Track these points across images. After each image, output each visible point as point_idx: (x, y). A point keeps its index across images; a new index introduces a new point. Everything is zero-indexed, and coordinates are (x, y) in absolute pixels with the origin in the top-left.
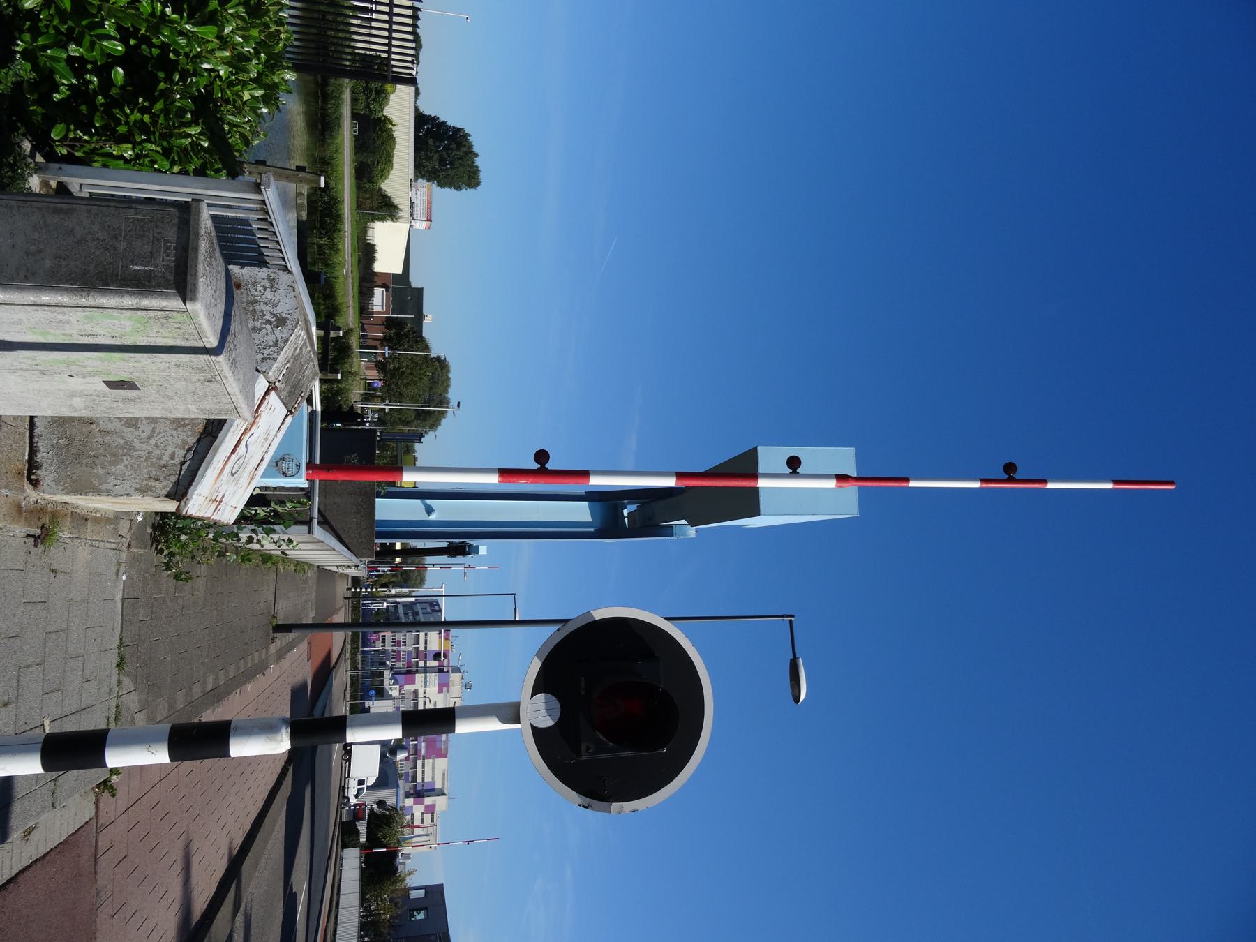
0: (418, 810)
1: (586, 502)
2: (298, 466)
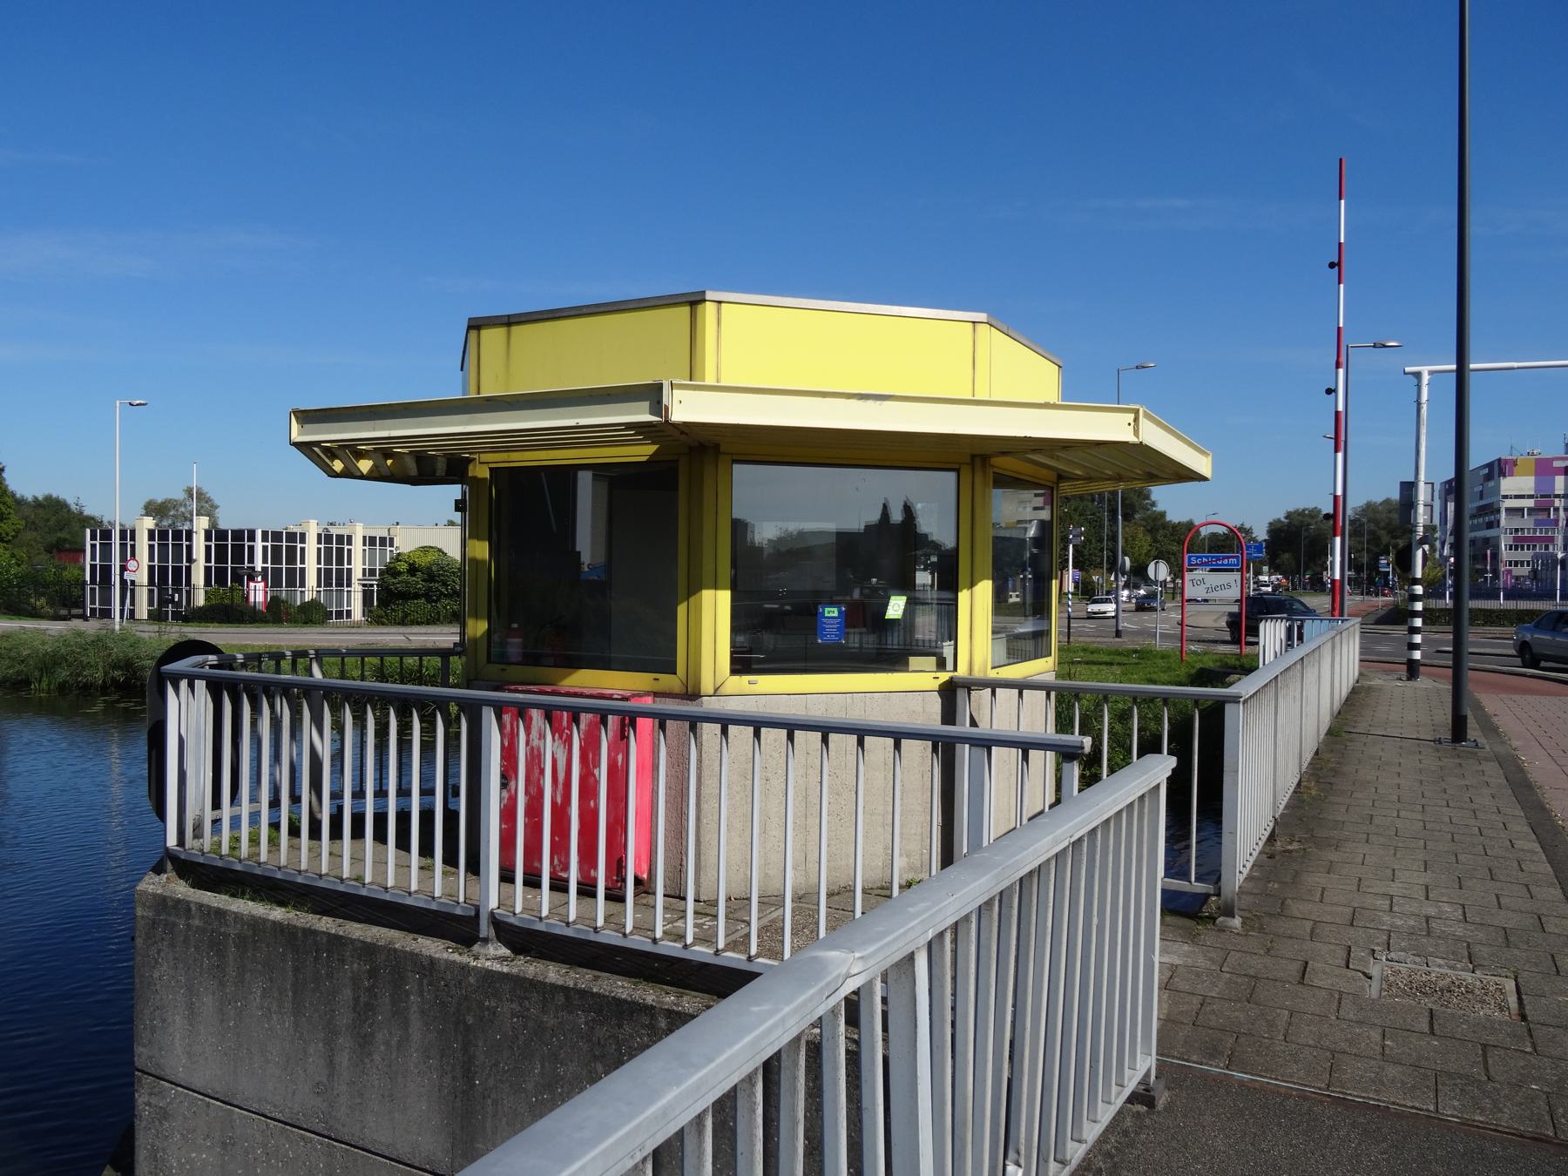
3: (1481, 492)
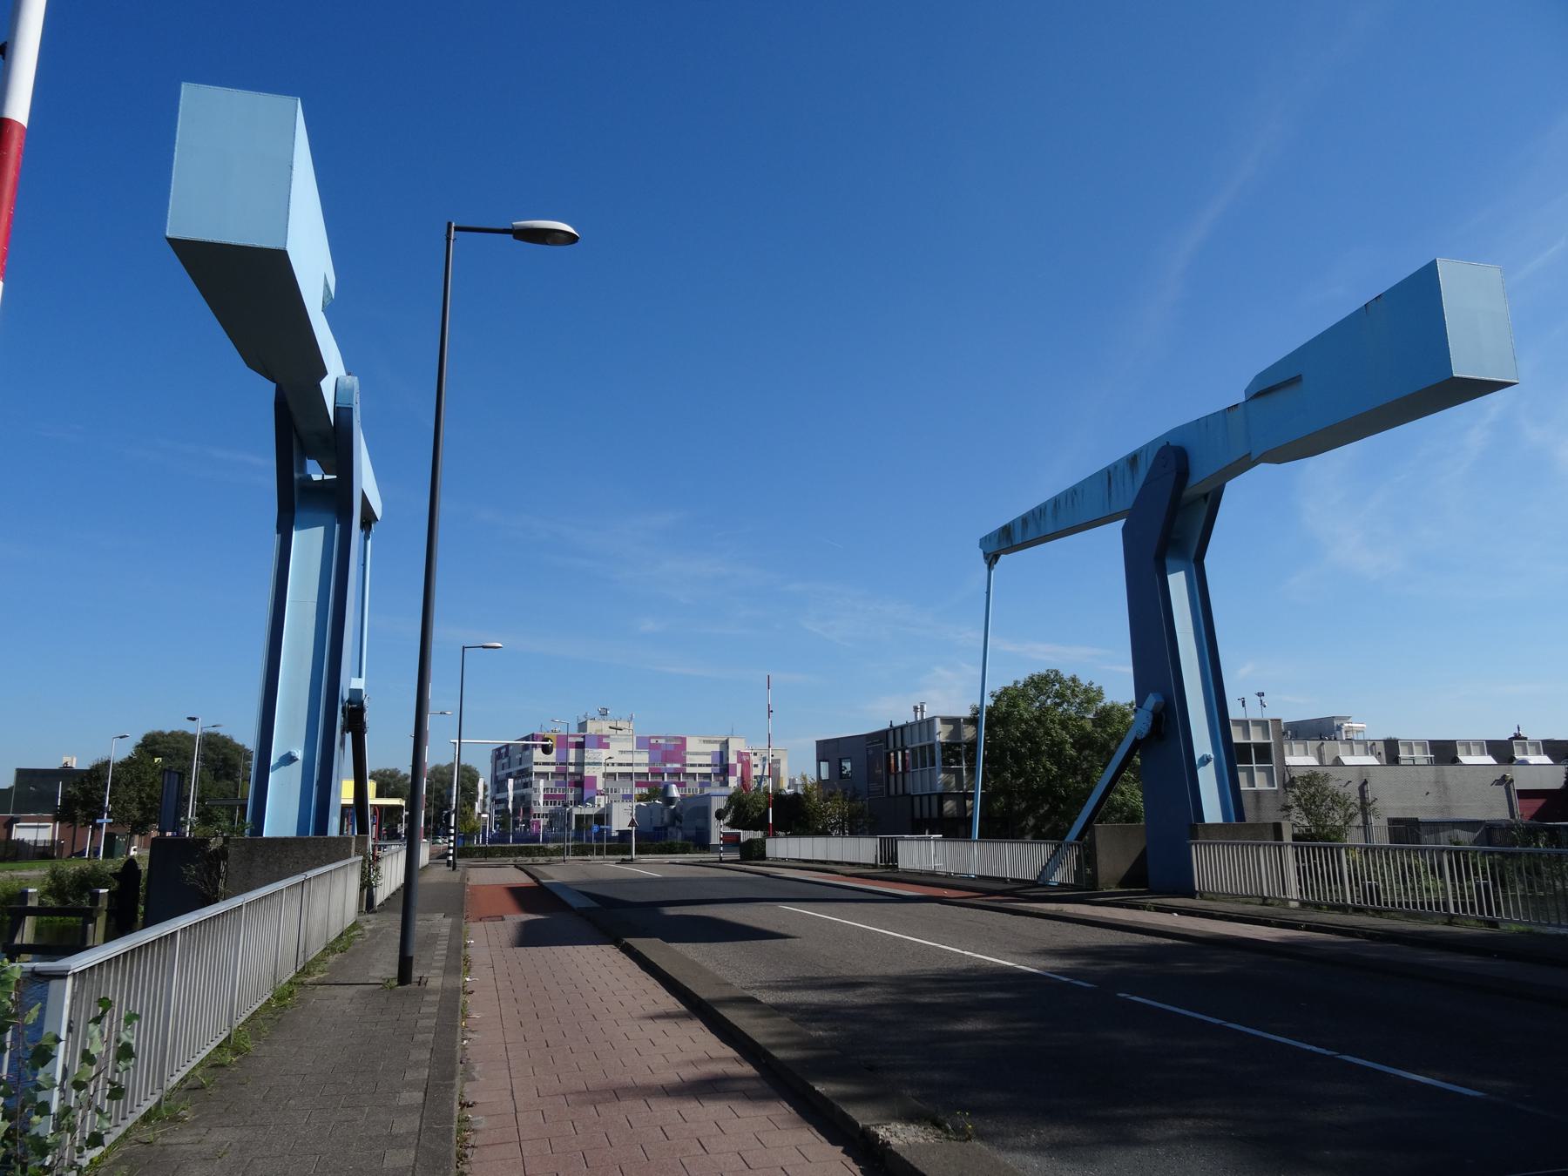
1: (294, 532)
3: (521, 759)
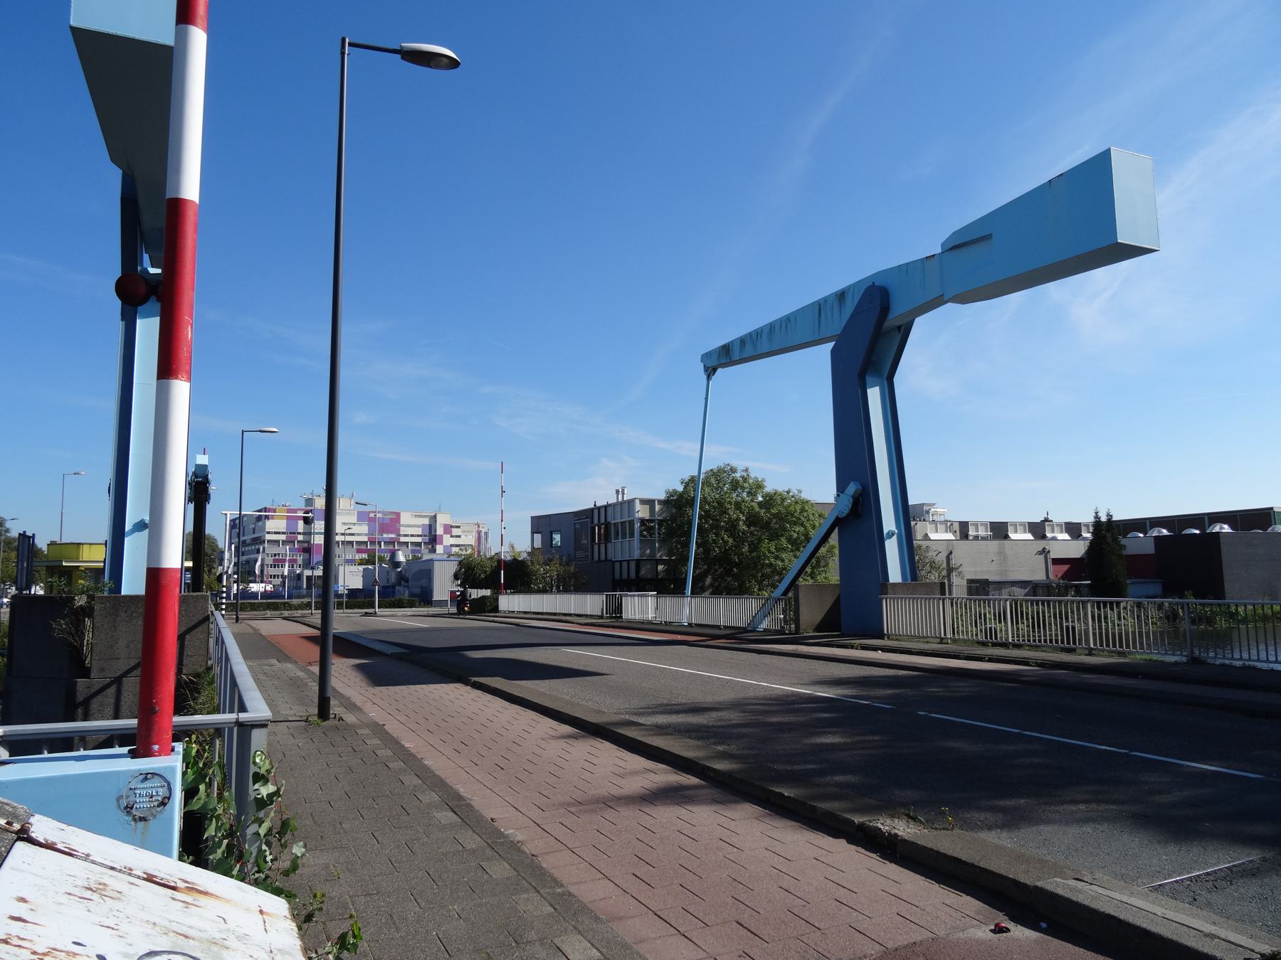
0: (448, 540)
1: (138, 320)
2: (146, 776)
3: (254, 528)
